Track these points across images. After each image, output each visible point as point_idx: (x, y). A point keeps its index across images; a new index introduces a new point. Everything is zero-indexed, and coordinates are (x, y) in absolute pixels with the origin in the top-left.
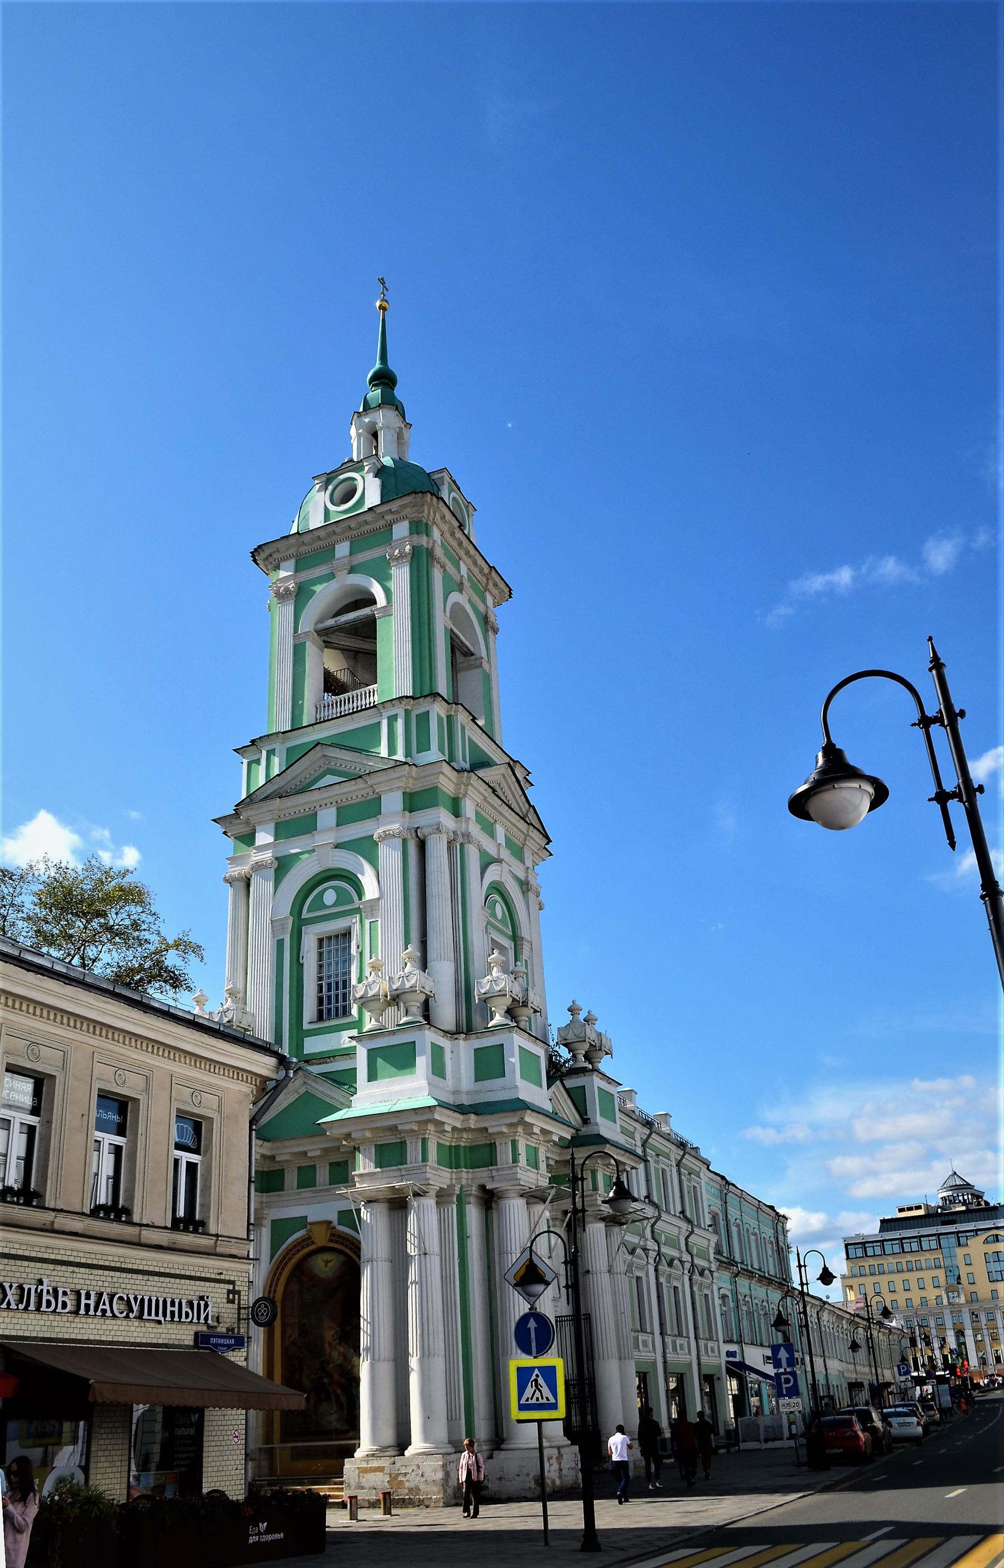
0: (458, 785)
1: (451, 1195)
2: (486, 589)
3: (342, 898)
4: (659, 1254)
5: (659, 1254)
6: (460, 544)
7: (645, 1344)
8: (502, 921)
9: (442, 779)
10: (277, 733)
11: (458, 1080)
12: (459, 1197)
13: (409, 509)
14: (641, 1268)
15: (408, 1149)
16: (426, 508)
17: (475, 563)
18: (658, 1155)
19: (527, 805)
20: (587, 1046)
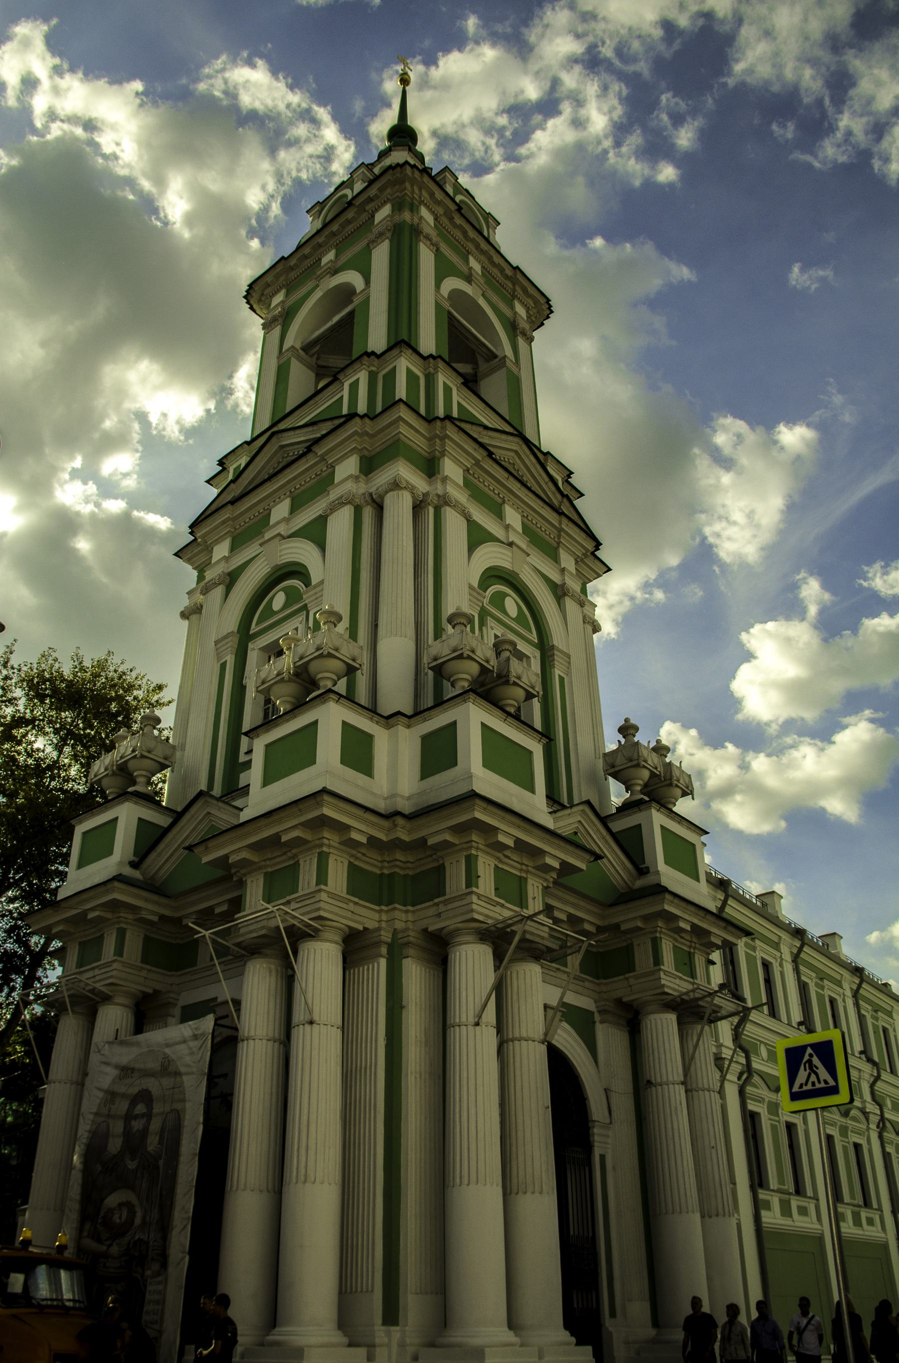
0: (430, 440)
1: (379, 943)
2: (514, 297)
3: (293, 596)
4: (882, 1118)
5: (882, 1118)
6: (465, 233)
7: (870, 1222)
8: (521, 618)
9: (403, 429)
10: (241, 445)
11: (394, 780)
12: (391, 947)
13: (389, 190)
14: (859, 1133)
15: (301, 871)
16: (408, 185)
17: (490, 258)
18: (876, 1011)
19: (559, 496)
20: (646, 774)
